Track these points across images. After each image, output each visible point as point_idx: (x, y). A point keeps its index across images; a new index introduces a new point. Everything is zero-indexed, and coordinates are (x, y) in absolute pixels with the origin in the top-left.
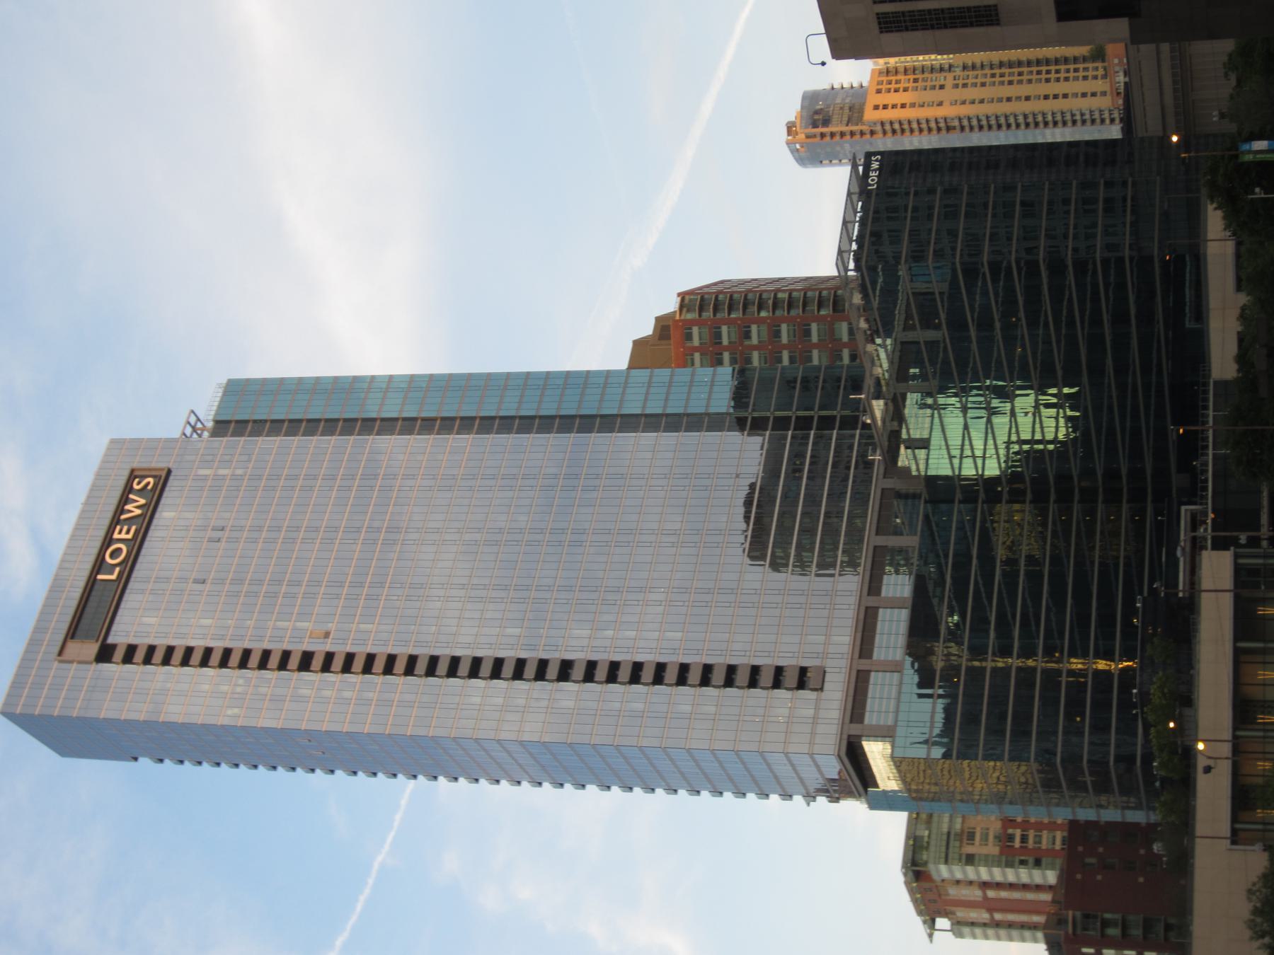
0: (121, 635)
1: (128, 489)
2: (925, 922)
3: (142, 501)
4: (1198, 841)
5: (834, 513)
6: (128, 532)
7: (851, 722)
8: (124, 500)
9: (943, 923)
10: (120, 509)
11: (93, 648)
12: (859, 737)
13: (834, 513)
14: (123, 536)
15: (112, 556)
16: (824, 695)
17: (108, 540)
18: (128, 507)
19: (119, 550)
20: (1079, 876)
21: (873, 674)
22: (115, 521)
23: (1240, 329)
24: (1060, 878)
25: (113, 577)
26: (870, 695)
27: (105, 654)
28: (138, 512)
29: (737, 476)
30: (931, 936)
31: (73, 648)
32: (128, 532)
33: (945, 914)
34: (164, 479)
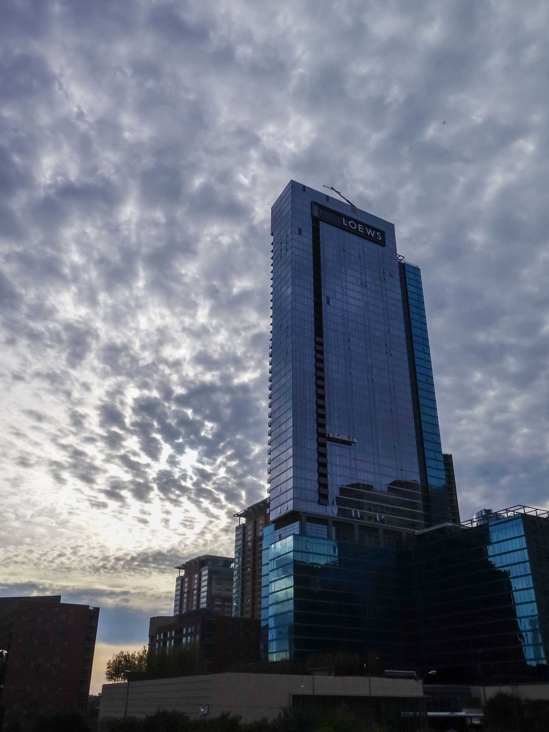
0: (322, 225)
1: (377, 230)
2: (183, 565)
3: (373, 235)
4: (368, 678)
5: (400, 512)
6: (361, 230)
7: (333, 521)
8: (373, 229)
9: (183, 573)
10: (369, 227)
11: (316, 214)
12: (300, 520)
13: (400, 512)
14: (359, 228)
15: (354, 227)
16: (317, 506)
17: (358, 222)
18: (370, 230)
19: (354, 227)
20: (26, 608)
21: (326, 526)
22: (365, 225)
23: (270, 721)
24: (203, 609)
25: (344, 223)
26: (312, 524)
27: (316, 221)
28: (369, 234)
29: (402, 470)
30: (178, 568)
31: (316, 208)
32: (361, 230)
33: (186, 575)
34: (382, 243)
